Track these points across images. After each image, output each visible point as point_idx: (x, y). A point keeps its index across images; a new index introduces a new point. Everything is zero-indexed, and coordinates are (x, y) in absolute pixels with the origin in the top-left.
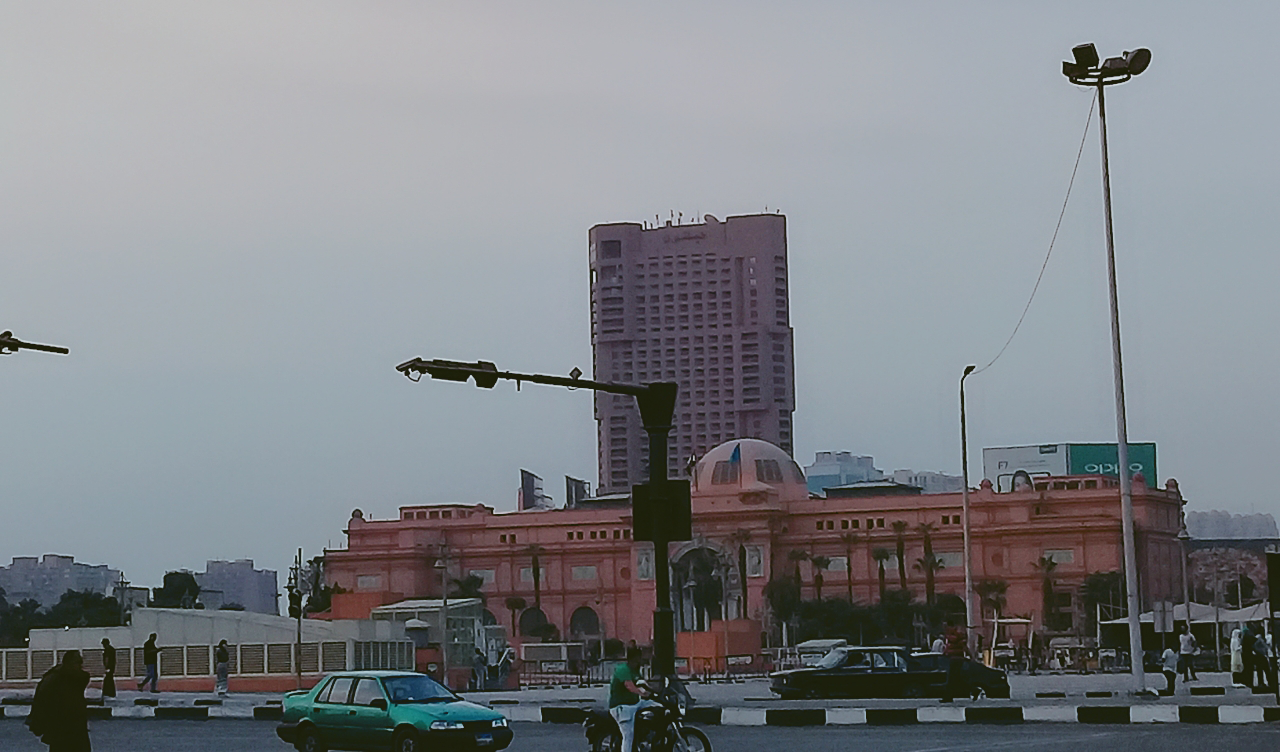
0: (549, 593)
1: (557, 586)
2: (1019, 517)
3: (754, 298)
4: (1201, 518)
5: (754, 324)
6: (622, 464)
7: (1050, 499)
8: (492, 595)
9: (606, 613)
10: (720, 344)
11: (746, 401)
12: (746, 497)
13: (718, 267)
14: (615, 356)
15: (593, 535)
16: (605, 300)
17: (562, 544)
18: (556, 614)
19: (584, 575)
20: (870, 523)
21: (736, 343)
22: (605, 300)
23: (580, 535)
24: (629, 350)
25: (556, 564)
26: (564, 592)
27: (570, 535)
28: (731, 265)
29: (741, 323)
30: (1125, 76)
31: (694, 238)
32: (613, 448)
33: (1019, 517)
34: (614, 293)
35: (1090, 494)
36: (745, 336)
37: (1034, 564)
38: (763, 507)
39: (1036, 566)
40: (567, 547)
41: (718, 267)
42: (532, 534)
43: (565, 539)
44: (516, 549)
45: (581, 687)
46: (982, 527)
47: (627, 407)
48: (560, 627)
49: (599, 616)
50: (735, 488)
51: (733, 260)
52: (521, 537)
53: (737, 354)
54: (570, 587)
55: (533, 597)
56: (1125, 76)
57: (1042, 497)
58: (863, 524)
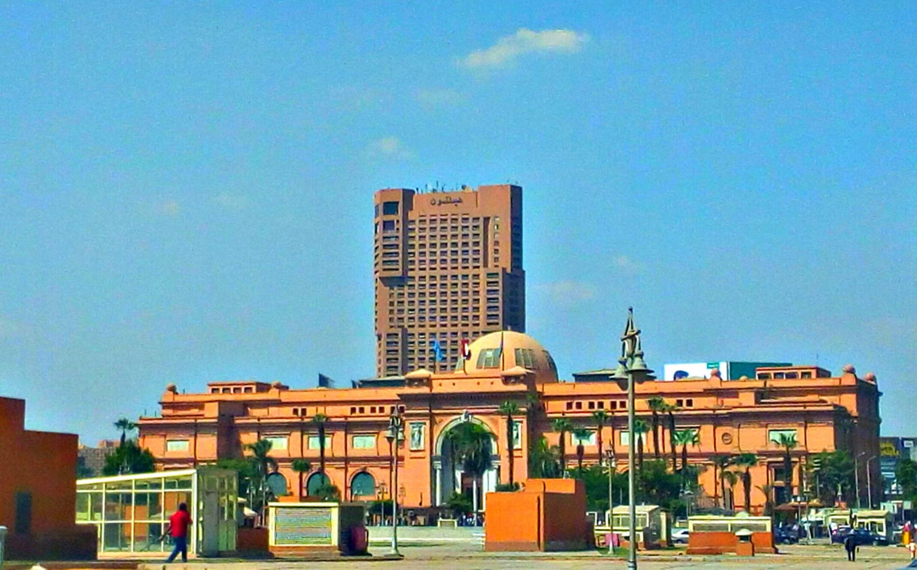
0: (334, 459)
1: (340, 453)
2: (747, 400)
3: (496, 256)
4: (828, 425)
5: (496, 266)
6: (394, 344)
7: (772, 387)
8: (283, 460)
9: (380, 474)
10: (438, 282)
11: (489, 324)
12: (507, 379)
13: (470, 223)
14: (391, 295)
15: (373, 410)
16: (385, 254)
17: (346, 417)
18: (336, 477)
19: (364, 444)
20: (613, 405)
21: (483, 280)
22: (385, 246)
23: (362, 410)
24: (402, 292)
25: (340, 434)
26: (347, 460)
27: (353, 410)
28: (481, 223)
29: (486, 265)
30: (366, 533)
31: (454, 202)
32: (389, 365)
33: (747, 400)
34: (393, 241)
35: (805, 383)
36: (489, 275)
37: (775, 441)
38: (425, 390)
39: (778, 443)
40: (350, 419)
41: (470, 223)
42: (321, 410)
43: (348, 413)
44: (306, 420)
45: (405, 496)
46: (714, 410)
47: (399, 327)
48: (341, 488)
49: (375, 478)
50: (499, 372)
51: (482, 220)
52: (311, 411)
53: (483, 288)
54: (351, 453)
55: (319, 463)
56: (366, 533)
57: (765, 384)
58: (607, 403)
